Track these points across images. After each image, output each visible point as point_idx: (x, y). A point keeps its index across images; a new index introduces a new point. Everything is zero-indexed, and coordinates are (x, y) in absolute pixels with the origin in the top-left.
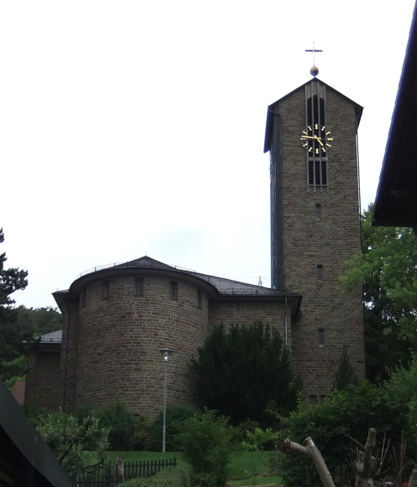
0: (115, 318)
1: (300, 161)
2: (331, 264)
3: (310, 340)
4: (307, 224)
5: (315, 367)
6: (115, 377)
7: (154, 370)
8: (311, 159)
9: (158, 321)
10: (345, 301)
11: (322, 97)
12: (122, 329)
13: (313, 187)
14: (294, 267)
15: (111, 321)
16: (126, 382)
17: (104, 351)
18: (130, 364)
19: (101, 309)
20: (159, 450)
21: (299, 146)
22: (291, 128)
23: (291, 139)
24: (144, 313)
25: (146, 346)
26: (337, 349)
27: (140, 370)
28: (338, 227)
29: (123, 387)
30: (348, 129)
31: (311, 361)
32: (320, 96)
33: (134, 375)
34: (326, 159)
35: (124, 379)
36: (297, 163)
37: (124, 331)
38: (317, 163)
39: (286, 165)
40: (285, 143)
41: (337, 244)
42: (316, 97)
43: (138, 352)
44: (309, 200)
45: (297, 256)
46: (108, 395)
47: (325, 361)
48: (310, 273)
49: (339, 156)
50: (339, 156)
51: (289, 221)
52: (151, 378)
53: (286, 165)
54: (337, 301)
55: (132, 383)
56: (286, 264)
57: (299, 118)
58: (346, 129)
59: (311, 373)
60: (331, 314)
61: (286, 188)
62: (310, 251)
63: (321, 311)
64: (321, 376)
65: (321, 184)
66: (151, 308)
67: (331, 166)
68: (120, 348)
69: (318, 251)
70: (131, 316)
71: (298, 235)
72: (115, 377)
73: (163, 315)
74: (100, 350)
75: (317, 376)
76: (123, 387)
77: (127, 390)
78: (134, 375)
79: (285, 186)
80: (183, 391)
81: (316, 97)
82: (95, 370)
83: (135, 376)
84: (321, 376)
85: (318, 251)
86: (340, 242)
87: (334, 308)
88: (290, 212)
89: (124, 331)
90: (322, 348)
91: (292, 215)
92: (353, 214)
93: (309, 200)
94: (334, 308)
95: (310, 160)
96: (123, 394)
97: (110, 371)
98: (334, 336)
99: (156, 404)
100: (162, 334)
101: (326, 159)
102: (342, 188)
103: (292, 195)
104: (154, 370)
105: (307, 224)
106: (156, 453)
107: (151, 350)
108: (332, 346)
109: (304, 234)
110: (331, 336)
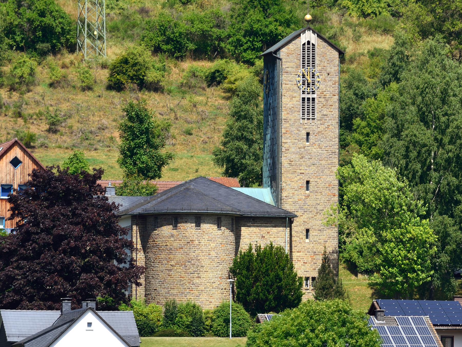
0: (182, 243)
1: (295, 97)
2: (316, 180)
3: (299, 237)
4: (299, 148)
5: (302, 257)
6: (184, 282)
7: (208, 277)
8: (303, 96)
9: (210, 245)
10: (325, 208)
11: (314, 43)
12: (188, 250)
13: (304, 119)
14: (289, 182)
15: (180, 245)
16: (191, 285)
17: (176, 264)
18: (194, 273)
19: (172, 236)
20: (228, 336)
21: (295, 85)
22: (289, 69)
23: (289, 78)
24: (202, 240)
25: (203, 262)
26: (319, 243)
27: (200, 277)
28: (322, 151)
29: (189, 289)
30: (333, 70)
31: (300, 252)
32: (312, 41)
33: (197, 281)
34: (315, 96)
35: (190, 283)
36: (294, 99)
37: (189, 252)
38: (308, 99)
39: (284, 100)
40: (284, 82)
41: (321, 164)
42: (309, 43)
43: (199, 266)
44: (301, 129)
45: (292, 173)
46: (179, 292)
47: (309, 252)
48: (300, 187)
49: (325, 93)
50: (325, 93)
51: (286, 146)
52: (208, 283)
53: (284, 100)
54: (320, 208)
55: (195, 286)
56: (283, 179)
57: (296, 60)
58: (331, 70)
59: (300, 261)
60: (315, 217)
61: (284, 119)
62: (301, 170)
63: (308, 216)
64: (306, 263)
65: (306, 117)
66: (206, 237)
67: (319, 102)
68: (187, 263)
69: (307, 170)
70: (193, 243)
71: (292, 157)
72: (184, 282)
73: (214, 241)
74: (173, 263)
75: (304, 263)
76: (189, 289)
77: (192, 290)
78: (197, 281)
79: (283, 117)
80: (225, 289)
81: (309, 43)
82: (169, 276)
83: (197, 282)
84: (306, 263)
85: (307, 170)
86: (323, 162)
87: (317, 213)
88: (287, 139)
89: (189, 252)
90: (308, 243)
91: (288, 141)
92: (334, 140)
93: (301, 129)
94: (317, 213)
95: (303, 97)
96: (190, 293)
97: (181, 277)
98: (316, 234)
99: (210, 299)
100: (213, 253)
101: (315, 96)
102: (326, 120)
103: (289, 125)
104: (208, 277)
105: (299, 148)
106: (11, 159)
107: (206, 264)
108: (315, 241)
109: (297, 156)
110: (314, 234)
